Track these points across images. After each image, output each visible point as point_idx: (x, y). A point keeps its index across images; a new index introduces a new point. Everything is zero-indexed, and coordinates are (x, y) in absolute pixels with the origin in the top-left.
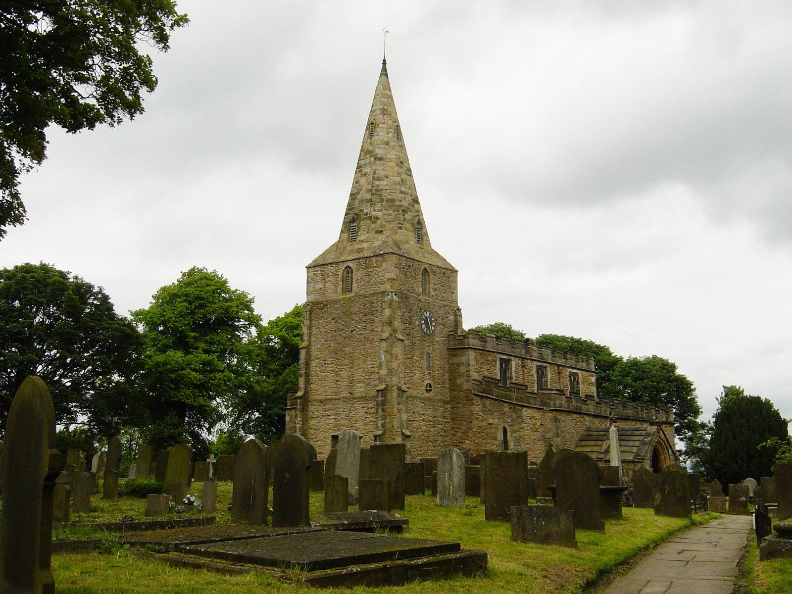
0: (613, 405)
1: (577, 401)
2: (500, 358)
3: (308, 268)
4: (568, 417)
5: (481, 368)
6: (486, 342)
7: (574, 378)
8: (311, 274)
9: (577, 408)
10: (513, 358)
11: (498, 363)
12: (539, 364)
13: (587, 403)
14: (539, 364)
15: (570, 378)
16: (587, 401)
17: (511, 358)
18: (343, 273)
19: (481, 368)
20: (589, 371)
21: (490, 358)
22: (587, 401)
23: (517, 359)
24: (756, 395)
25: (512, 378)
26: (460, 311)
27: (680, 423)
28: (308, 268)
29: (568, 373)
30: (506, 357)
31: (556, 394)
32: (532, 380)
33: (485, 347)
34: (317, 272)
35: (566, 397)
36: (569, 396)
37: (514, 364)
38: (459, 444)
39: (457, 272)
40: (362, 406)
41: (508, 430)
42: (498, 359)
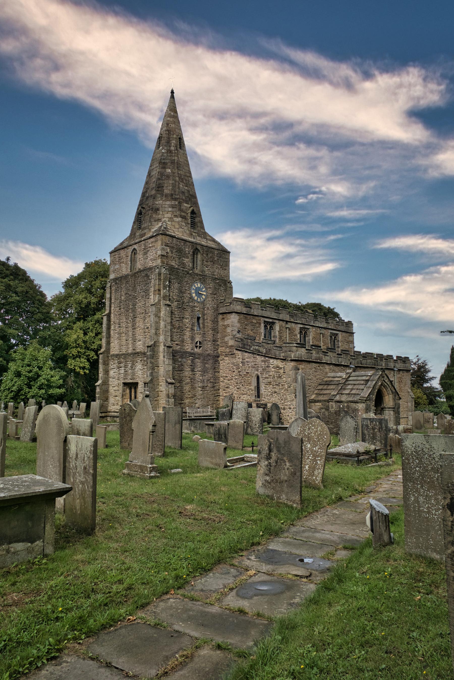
0: (354, 356)
1: (318, 353)
2: (265, 321)
3: (111, 253)
4: (308, 365)
5: (245, 328)
6: (251, 308)
7: (335, 337)
8: (112, 258)
9: (319, 358)
10: (277, 321)
11: (263, 325)
12: (302, 326)
13: (328, 354)
14: (302, 326)
15: (331, 337)
16: (327, 353)
17: (275, 321)
18: (131, 255)
19: (245, 328)
20: (348, 332)
21: (254, 321)
22: (327, 353)
23: (281, 322)
24: (306, 303)
25: (276, 337)
26: (231, 284)
27: (5, 308)
28: (111, 253)
29: (329, 333)
30: (271, 320)
31: (296, 347)
32: (295, 339)
33: (250, 311)
34: (151, 245)
35: (307, 350)
36: (353, 355)
37: (277, 327)
38: (226, 389)
39: (229, 252)
40: (140, 359)
41: (260, 377)
42: (262, 322)
